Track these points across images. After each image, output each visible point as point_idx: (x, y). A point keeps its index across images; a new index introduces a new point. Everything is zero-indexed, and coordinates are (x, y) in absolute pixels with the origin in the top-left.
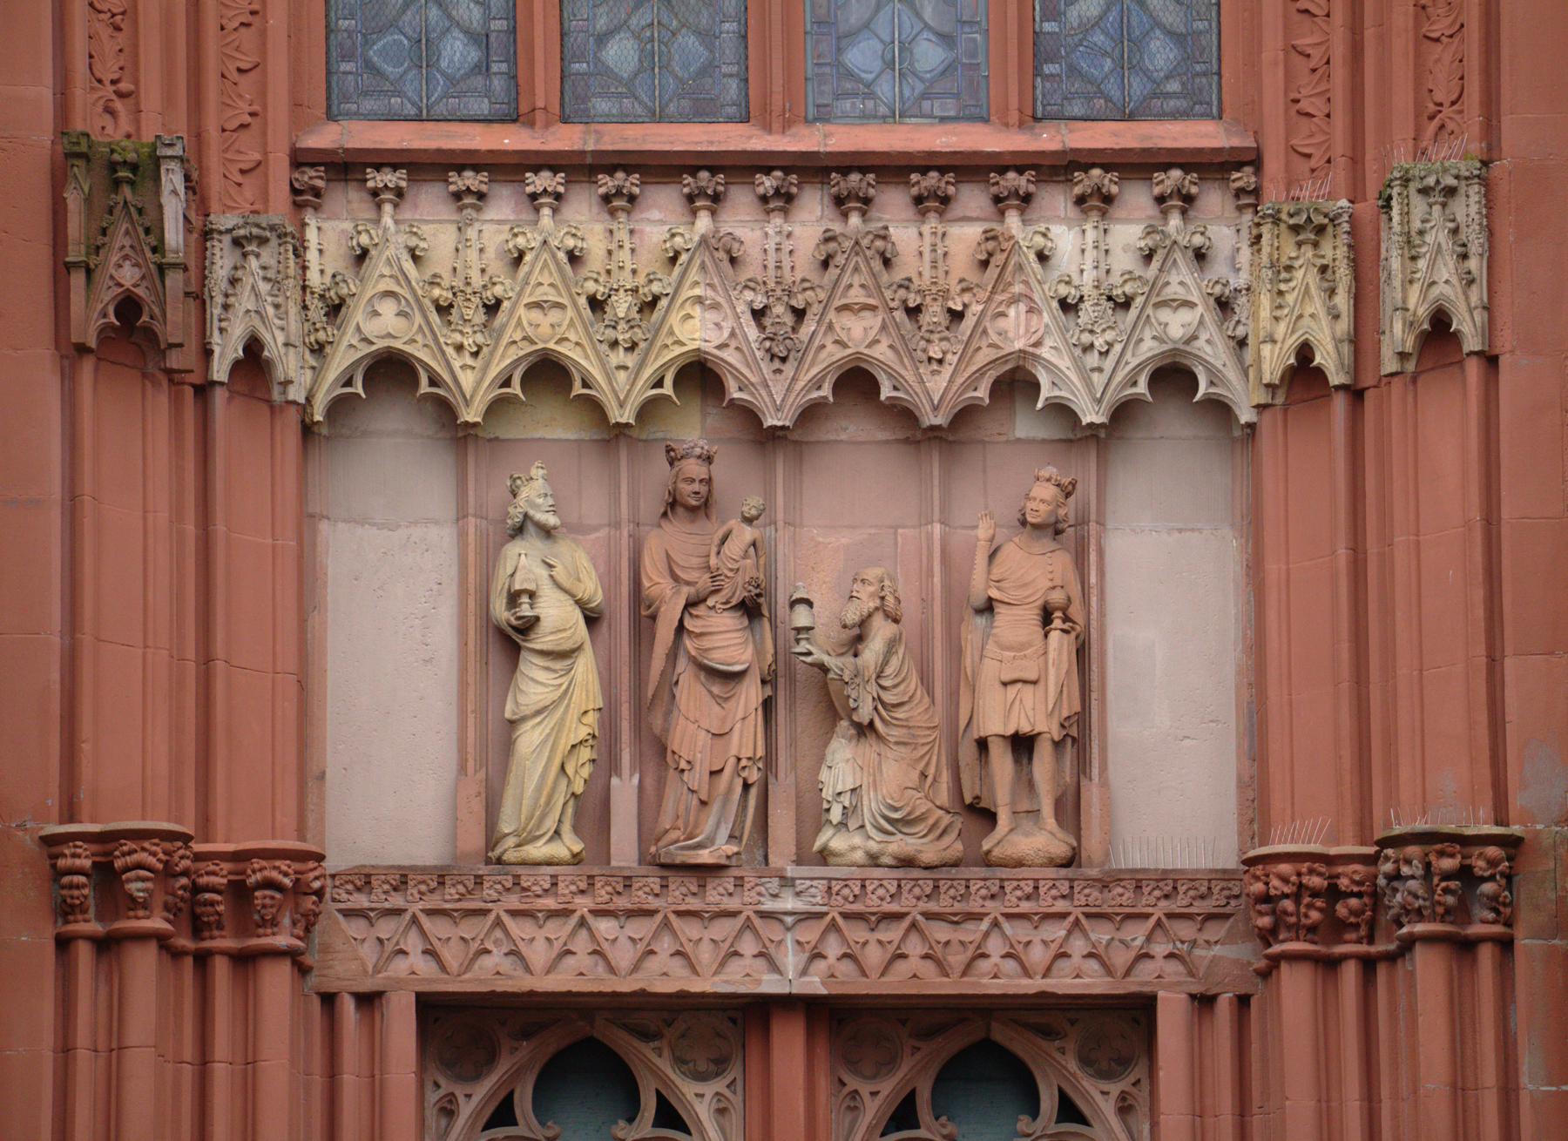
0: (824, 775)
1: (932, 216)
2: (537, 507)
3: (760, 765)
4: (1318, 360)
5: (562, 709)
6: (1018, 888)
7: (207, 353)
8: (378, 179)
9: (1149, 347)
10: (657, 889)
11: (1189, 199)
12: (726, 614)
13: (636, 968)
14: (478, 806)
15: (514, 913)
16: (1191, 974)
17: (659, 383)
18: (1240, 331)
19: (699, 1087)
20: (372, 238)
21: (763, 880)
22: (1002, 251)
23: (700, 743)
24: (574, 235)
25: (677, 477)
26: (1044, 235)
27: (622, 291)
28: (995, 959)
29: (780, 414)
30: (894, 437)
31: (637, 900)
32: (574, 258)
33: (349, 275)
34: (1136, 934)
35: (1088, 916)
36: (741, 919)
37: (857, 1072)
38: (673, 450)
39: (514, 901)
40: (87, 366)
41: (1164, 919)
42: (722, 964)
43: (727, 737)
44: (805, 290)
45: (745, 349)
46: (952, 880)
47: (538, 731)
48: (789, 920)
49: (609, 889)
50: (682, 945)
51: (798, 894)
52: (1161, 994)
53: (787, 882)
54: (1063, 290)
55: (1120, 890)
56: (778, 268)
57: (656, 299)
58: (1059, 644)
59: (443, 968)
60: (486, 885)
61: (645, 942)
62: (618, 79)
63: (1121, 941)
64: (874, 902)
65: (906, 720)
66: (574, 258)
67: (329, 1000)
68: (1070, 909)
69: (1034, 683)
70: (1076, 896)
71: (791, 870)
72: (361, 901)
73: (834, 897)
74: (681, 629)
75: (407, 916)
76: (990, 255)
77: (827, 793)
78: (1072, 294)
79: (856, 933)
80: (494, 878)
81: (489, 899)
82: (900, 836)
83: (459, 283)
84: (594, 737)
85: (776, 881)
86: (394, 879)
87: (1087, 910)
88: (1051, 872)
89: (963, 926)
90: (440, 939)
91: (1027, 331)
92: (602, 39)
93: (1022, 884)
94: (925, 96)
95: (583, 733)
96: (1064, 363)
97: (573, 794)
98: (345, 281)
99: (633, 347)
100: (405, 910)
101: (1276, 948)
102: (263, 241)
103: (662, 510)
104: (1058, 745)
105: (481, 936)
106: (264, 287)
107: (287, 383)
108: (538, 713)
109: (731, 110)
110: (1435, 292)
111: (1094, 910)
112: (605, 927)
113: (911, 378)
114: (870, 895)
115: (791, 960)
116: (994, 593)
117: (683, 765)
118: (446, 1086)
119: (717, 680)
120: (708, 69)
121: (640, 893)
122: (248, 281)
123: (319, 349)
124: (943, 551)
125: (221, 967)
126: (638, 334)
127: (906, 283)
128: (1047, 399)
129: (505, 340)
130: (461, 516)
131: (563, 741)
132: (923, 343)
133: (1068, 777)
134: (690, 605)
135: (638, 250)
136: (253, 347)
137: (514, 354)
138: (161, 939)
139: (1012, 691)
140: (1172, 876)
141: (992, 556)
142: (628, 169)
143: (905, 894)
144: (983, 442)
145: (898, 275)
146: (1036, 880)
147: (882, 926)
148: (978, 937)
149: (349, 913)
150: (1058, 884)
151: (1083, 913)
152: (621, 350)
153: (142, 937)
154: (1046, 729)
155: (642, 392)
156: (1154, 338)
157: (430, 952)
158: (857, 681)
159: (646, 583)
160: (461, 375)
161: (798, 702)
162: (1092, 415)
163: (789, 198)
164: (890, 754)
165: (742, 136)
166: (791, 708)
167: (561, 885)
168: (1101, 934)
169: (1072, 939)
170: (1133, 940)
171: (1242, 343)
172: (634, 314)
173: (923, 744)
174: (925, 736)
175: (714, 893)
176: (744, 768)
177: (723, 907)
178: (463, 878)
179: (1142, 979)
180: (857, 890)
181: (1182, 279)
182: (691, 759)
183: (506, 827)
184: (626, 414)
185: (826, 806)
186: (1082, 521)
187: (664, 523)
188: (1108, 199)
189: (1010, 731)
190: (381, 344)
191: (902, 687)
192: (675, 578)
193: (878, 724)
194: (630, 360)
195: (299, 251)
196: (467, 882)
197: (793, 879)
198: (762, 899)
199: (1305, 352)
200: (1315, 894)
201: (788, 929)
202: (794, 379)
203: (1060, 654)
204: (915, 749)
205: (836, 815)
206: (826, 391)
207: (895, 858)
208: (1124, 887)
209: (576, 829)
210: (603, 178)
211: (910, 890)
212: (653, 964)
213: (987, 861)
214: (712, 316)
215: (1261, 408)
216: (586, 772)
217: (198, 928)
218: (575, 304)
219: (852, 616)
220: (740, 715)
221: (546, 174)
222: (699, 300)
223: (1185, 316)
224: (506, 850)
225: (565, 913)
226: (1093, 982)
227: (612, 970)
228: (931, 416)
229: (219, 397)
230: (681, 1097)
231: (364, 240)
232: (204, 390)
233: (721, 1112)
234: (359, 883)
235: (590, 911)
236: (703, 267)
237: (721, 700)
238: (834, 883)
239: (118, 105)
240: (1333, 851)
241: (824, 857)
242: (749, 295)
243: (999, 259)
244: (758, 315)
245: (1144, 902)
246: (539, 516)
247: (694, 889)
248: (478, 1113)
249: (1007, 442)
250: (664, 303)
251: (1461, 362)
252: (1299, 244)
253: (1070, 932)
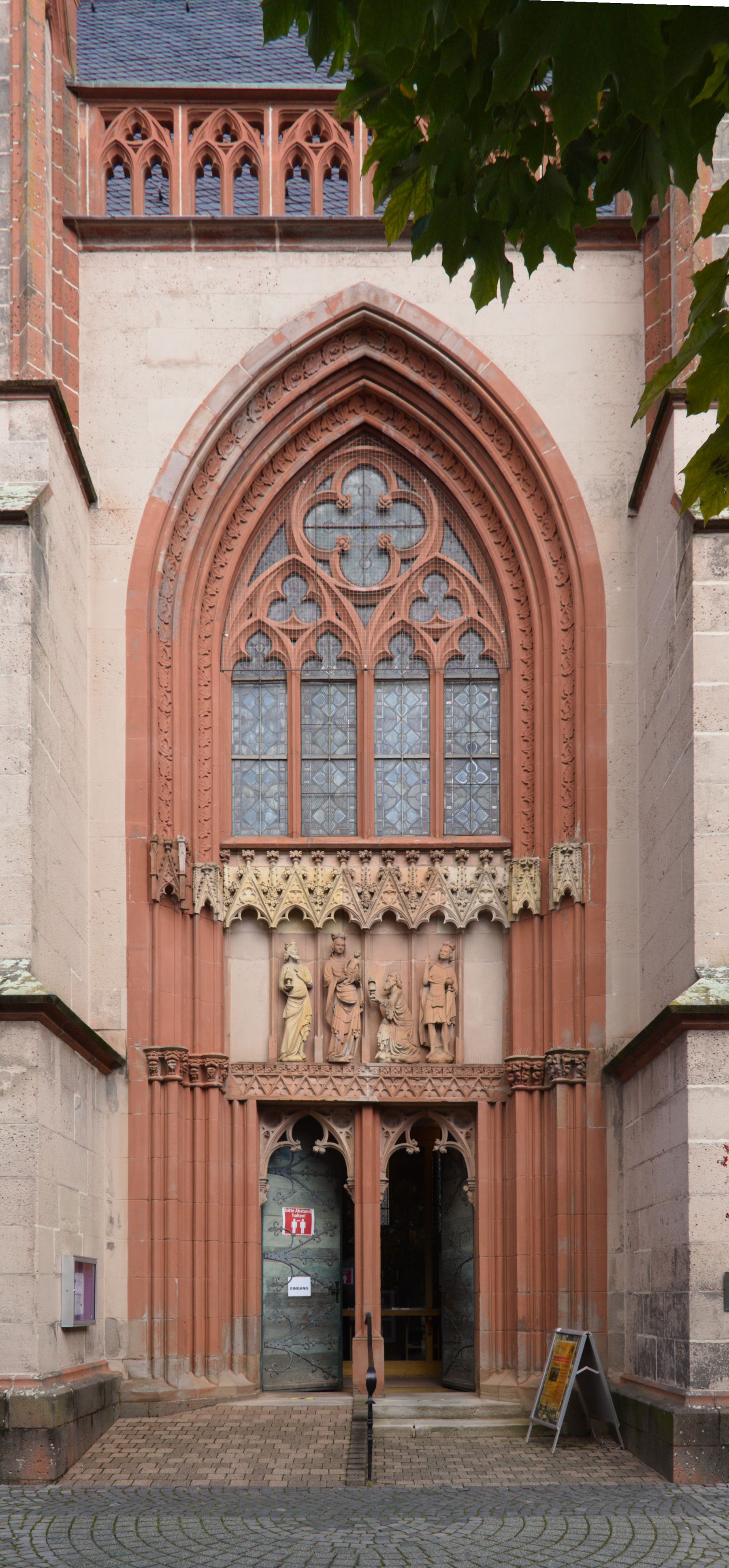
0: (379, 1035)
1: (413, 864)
4: (530, 906)
7: (194, 905)
8: (245, 853)
9: (478, 904)
11: (490, 859)
13: (322, 1093)
14: (275, 1045)
15: (286, 1077)
16: (488, 1096)
17: (330, 916)
18: (506, 899)
19: (341, 1130)
28: (429, 1091)
32: (304, 878)
33: (237, 882)
34: (472, 1083)
37: (387, 1126)
39: (285, 1073)
40: (157, 906)
42: (348, 1092)
52: (479, 1102)
53: (368, 1068)
54: (452, 886)
57: (329, 889)
58: (450, 995)
59: (264, 1093)
62: (318, 823)
64: (393, 1074)
66: (304, 878)
67: (231, 1102)
71: (368, 1064)
72: (240, 1072)
74: (336, 990)
77: (380, 1041)
78: (455, 888)
79: (387, 1083)
83: (269, 885)
86: (250, 1066)
88: (447, 1065)
92: (313, 812)
94: (411, 828)
95: (306, 1022)
96: (452, 909)
99: (322, 904)
101: (514, 1087)
102: (210, 870)
106: (211, 884)
107: (217, 914)
109: (353, 833)
110: (566, 883)
115: (368, 1091)
116: (431, 980)
118: (267, 1129)
120: (345, 821)
122: (206, 883)
123: (228, 905)
125: (198, 1091)
126: (323, 900)
129: (284, 902)
130: (271, 956)
133: (452, 1036)
134: (338, 983)
136: (208, 902)
137: (286, 906)
138: (179, 1081)
141: (430, 969)
142: (321, 850)
145: (402, 882)
149: (237, 1076)
153: (173, 1080)
155: (324, 918)
157: (261, 1088)
162: (461, 925)
163: (369, 858)
166: (369, 1016)
168: (461, 1083)
171: (506, 903)
172: (322, 894)
179: (473, 1098)
181: (486, 884)
183: (283, 1051)
186: (457, 959)
188: (466, 859)
190: (246, 904)
192: (334, 975)
194: (320, 908)
195: (222, 875)
199: (526, 904)
200: (526, 1070)
205: (382, 1047)
206: (380, 918)
209: (304, 1051)
210: (313, 852)
212: (326, 1092)
213: (427, 1061)
214: (346, 895)
215: (512, 923)
216: (307, 1034)
217: (191, 1079)
219: (387, 987)
221: (296, 851)
222: (342, 890)
223: (489, 895)
225: (301, 1077)
226: (459, 1098)
227: (314, 1094)
229: (197, 917)
230: (335, 1133)
231: (241, 872)
232: (192, 916)
233: (348, 1137)
237: (347, 1012)
239: (168, 829)
240: (532, 1057)
241: (378, 1060)
242: (357, 888)
243: (433, 877)
244: (360, 894)
246: (294, 956)
248: (276, 1137)
251: (573, 906)
252: (524, 871)
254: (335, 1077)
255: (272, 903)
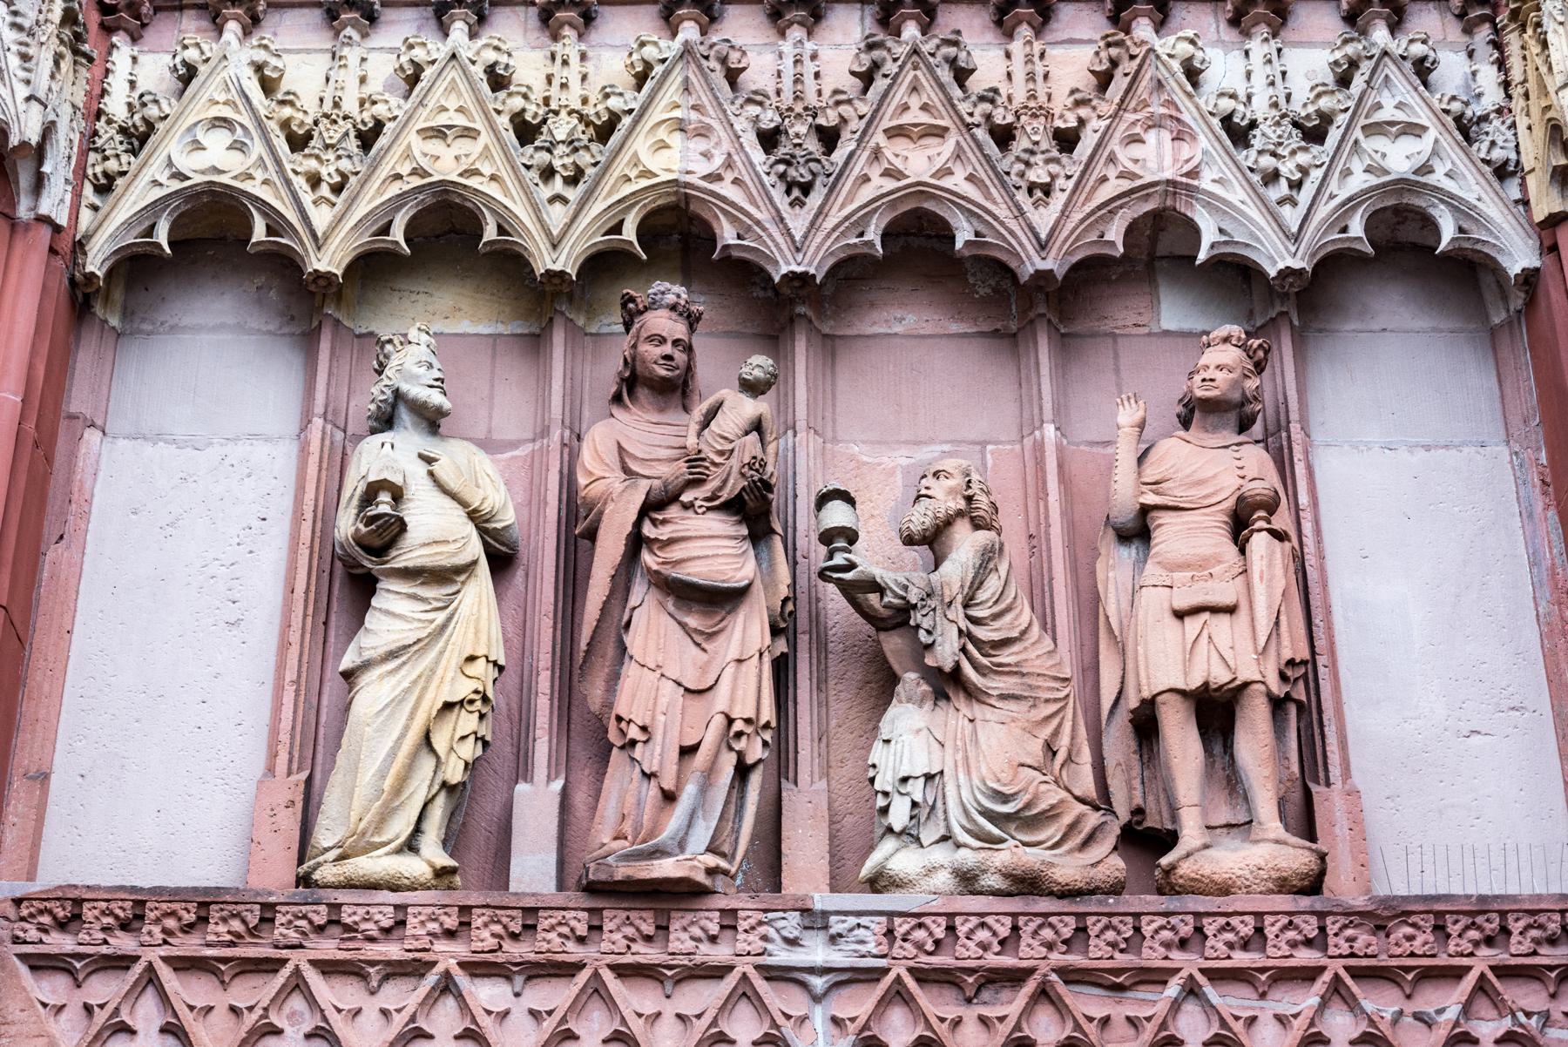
2: (413, 378)
3: (768, 736)
5: (432, 654)
6: (1227, 927)
10: (582, 930)
12: (710, 515)
15: (328, 968)
20: (202, 53)
21: (771, 915)
22: (1132, 57)
23: (663, 702)
24: (497, 48)
25: (638, 337)
26: (1192, 42)
27: (563, 113)
29: (799, 257)
30: (974, 330)
31: (545, 946)
35: (1357, 974)
36: (731, 980)
38: (632, 300)
41: (1490, 976)
43: (711, 693)
44: (838, 103)
45: (747, 179)
46: (1110, 915)
47: (394, 680)
48: (818, 983)
49: (498, 928)
50: (624, 1021)
51: (834, 939)
53: (815, 920)
55: (1409, 930)
56: (796, 81)
60: (280, 919)
61: (557, 1016)
63: (1418, 1017)
64: (966, 953)
65: (1017, 664)
68: (1324, 961)
69: (1231, 610)
70: (1331, 940)
71: (822, 900)
72: (62, 943)
73: (899, 942)
74: (637, 541)
75: (138, 969)
76: (1114, 63)
80: (295, 909)
81: (283, 941)
82: (1012, 842)
84: (485, 699)
85: (794, 918)
86: (124, 911)
87: (1352, 962)
88: (1284, 902)
89: (1130, 994)
90: (191, 1008)
91: (1175, 160)
93: (1235, 921)
97: (444, 785)
98: (156, 101)
100: (138, 958)
103: (614, 389)
104: (1277, 705)
105: (265, 1003)
108: (392, 655)
111: (1365, 962)
112: (487, 994)
113: (1002, 211)
114: (963, 940)
117: (634, 732)
119: (696, 607)
121: (552, 936)
124: (1060, 466)
126: (584, 159)
127: (991, 94)
128: (1213, 246)
129: (384, 171)
131: (429, 695)
132: (1021, 166)
134: (652, 507)
135: (591, 78)
139: (1193, 624)
140: (1496, 907)
143: (1026, 938)
144: (1114, 336)
146: (1259, 915)
147: (986, 995)
148: (1161, 1008)
150: (1297, 920)
151: (1346, 968)
152: (558, 180)
154: (1258, 677)
156: (1367, 171)
158: (932, 603)
159: (582, 480)
160: (312, 211)
161: (831, 683)
164: (988, 713)
165: (770, 955)
166: (821, 683)
167: (411, 921)
169: (1327, 1013)
170: (1440, 1012)
173: (1047, 701)
174: (1052, 689)
175: (685, 936)
176: (739, 735)
177: (698, 959)
178: (240, 908)
180: (940, 933)
182: (647, 722)
184: (563, 258)
185: (881, 802)
187: (616, 411)
189: (1195, 683)
191: (1008, 618)
192: (626, 470)
193: (968, 669)
196: (249, 917)
197: (825, 914)
198: (769, 947)
201: (817, 999)
202: (821, 212)
203: (1270, 565)
204: (1034, 706)
205: (899, 816)
207: (1006, 876)
208: (1414, 925)
211: (1035, 933)
214: (701, 145)
218: (493, 127)
220: (733, 653)
224: (319, 865)
228: (1037, 259)
234: (61, 914)
235: (462, 965)
236: (687, 88)
237: (701, 639)
238: (897, 921)
241: (878, 883)
244: (769, 140)
245: (1452, 949)
247: (648, 929)
249: (1149, 334)
250: (627, 121)
253: (1324, 1004)
254: (624, 972)
255: (328, 172)
